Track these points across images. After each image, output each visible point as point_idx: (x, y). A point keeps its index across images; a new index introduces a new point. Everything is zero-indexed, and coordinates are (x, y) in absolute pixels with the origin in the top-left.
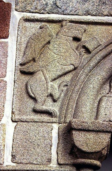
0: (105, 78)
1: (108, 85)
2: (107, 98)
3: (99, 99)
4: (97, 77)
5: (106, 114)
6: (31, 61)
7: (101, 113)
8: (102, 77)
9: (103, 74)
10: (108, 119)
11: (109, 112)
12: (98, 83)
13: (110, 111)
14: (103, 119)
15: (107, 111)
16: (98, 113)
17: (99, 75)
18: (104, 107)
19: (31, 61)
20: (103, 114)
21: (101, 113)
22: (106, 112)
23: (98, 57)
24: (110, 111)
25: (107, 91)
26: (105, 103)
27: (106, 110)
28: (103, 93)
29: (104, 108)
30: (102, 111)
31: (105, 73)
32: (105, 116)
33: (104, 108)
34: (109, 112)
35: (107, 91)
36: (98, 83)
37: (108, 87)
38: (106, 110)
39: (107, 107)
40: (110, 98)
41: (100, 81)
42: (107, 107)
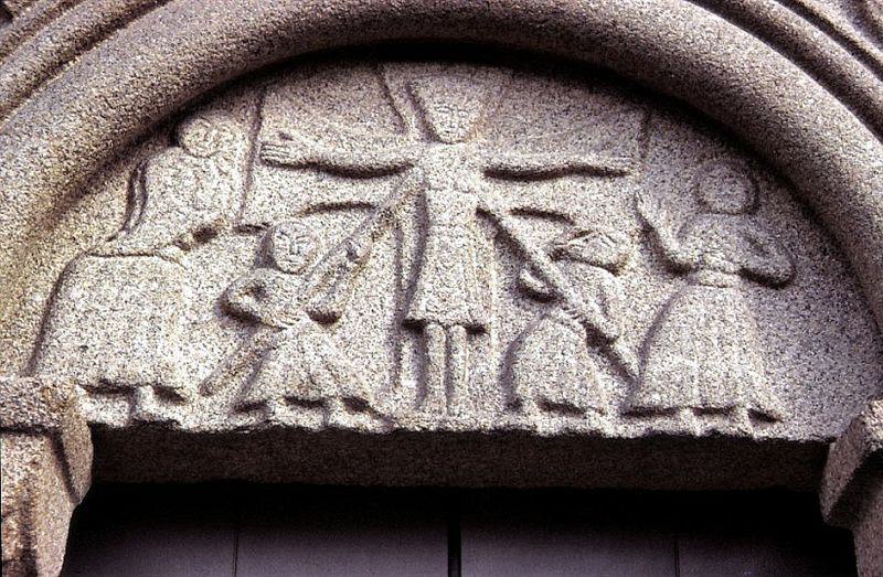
0: (77, 152)
1: (123, 191)
2: (102, 260)
3: (59, 267)
4: (27, 147)
5: (85, 348)
6: (148, 384)
7: (55, 343)
8: (57, 143)
9: (63, 129)
10: (93, 372)
11: (102, 333)
12: (32, 174)
13: (110, 330)
14: (64, 371)
15: (91, 329)
16: (43, 340)
17: (40, 135)
18: (78, 307)
19: (148, 384)
20: (65, 346)
21: (55, 343)
22: (84, 335)
23: (48, 42)
24: (110, 330)
25: (112, 225)
26: (86, 285)
27: (89, 323)
28: (87, 237)
29: (81, 315)
30: (65, 334)
31: (79, 122)
32: (77, 356)
33: (81, 315)
34: (102, 333)
35: (110, 228)
36: (32, 174)
37: (119, 206)
38: (89, 323)
39: (97, 306)
40: (120, 259)
41: (49, 164)
42: (97, 306)
